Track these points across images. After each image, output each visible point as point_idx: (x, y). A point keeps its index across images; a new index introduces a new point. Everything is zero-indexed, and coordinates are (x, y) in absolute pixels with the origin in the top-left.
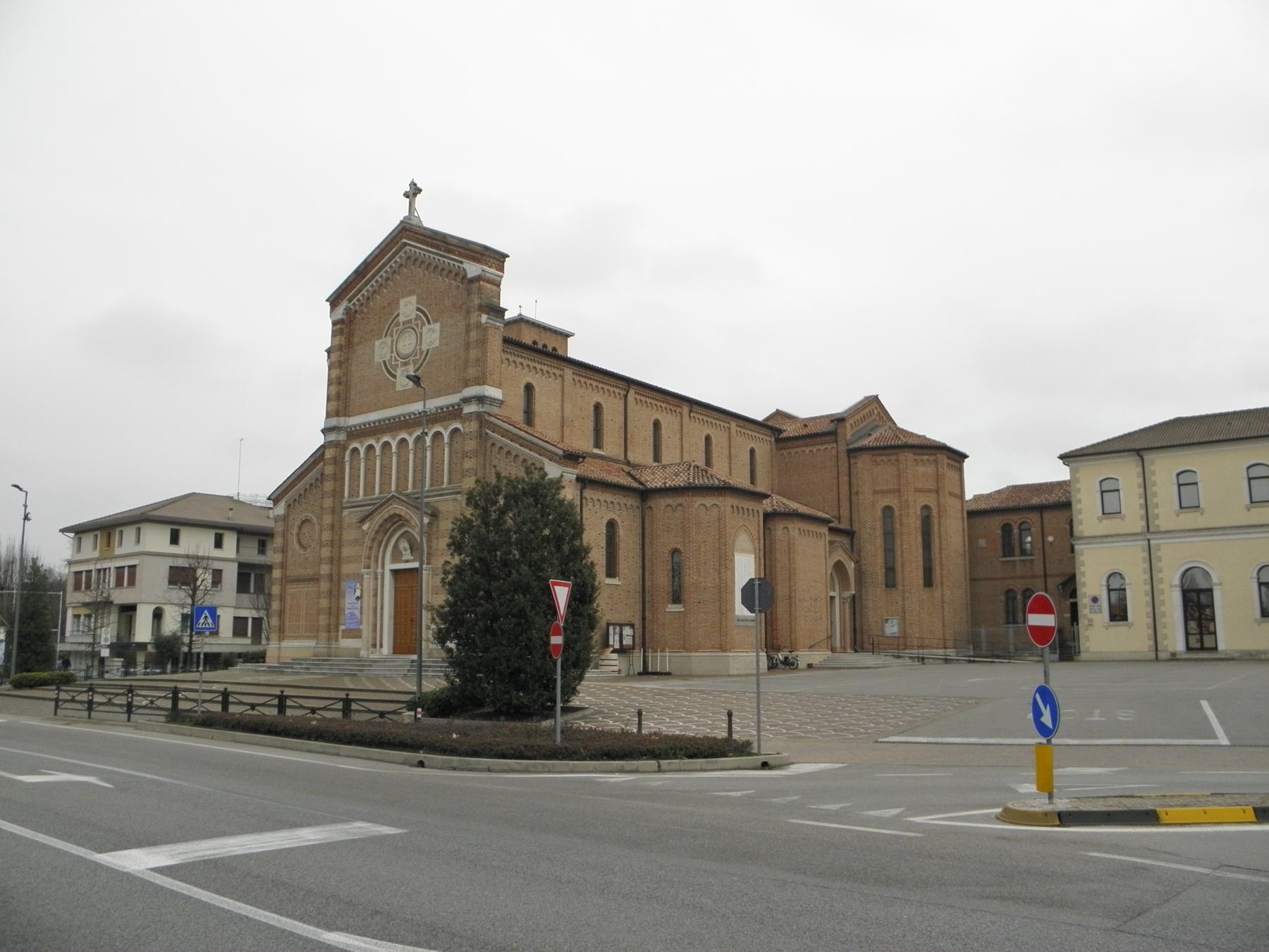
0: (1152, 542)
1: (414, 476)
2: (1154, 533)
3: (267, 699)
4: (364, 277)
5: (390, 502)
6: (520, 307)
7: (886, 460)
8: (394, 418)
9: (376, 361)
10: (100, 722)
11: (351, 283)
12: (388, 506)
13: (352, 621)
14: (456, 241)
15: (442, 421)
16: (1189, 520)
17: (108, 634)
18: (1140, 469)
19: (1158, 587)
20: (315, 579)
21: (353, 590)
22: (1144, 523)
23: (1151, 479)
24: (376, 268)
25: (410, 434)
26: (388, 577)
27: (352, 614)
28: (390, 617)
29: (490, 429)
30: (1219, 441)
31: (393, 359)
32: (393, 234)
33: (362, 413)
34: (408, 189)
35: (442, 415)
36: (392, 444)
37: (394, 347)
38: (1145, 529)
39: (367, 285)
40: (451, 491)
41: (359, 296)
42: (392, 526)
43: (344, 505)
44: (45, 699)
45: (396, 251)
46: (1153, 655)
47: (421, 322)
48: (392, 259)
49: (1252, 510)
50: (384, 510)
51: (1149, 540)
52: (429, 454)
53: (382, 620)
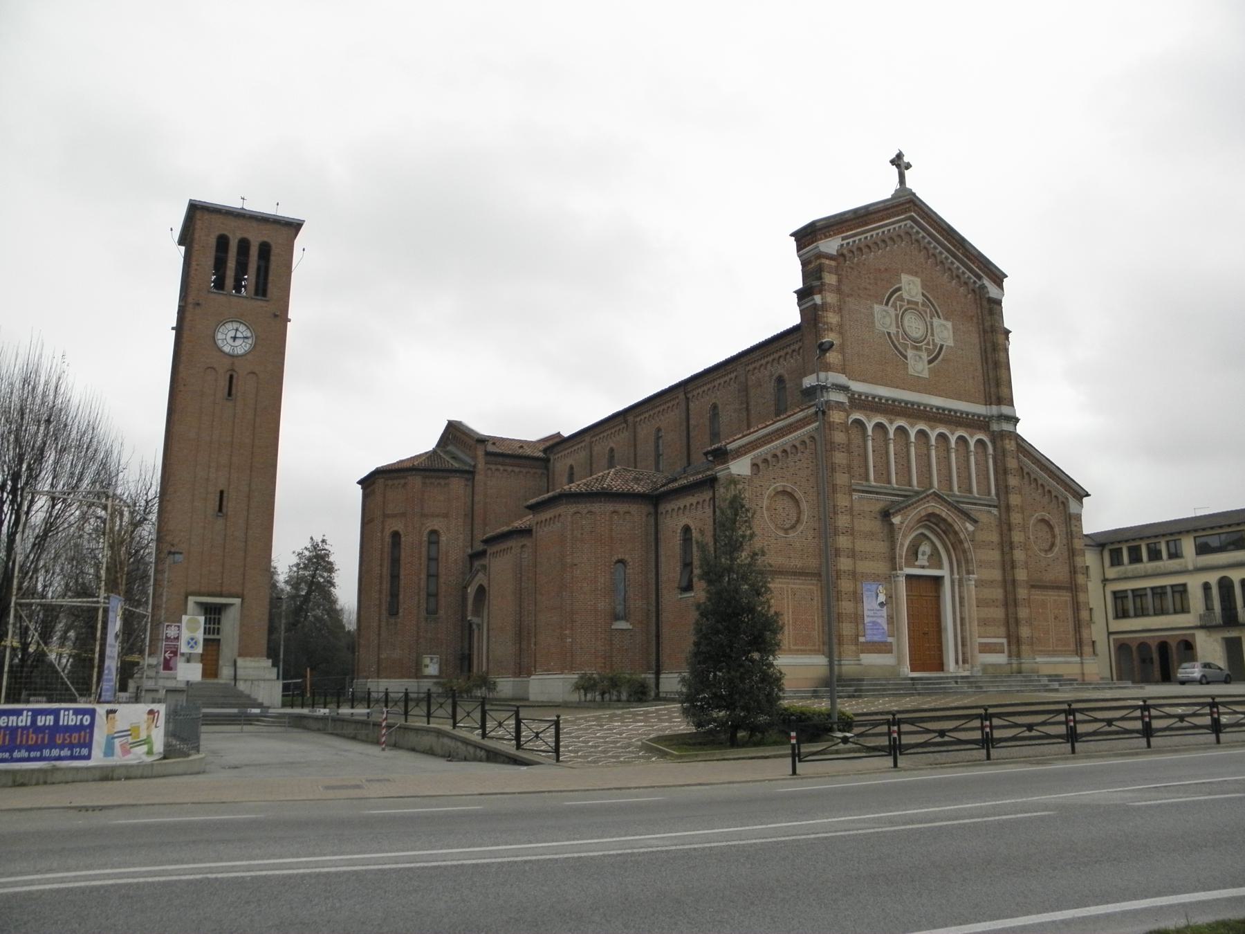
1: (996, 485)
3: (968, 725)
7: (436, 483)
8: (900, 401)
10: (1160, 751)
11: (847, 221)
12: (924, 503)
13: (875, 632)
15: (909, 417)
17: (197, 629)
21: (874, 596)
24: (946, 242)
26: (902, 583)
27: (874, 623)
28: (946, 629)
35: (857, 401)
36: (931, 435)
37: (929, 327)
40: (986, 503)
43: (854, 487)
53: (956, 636)
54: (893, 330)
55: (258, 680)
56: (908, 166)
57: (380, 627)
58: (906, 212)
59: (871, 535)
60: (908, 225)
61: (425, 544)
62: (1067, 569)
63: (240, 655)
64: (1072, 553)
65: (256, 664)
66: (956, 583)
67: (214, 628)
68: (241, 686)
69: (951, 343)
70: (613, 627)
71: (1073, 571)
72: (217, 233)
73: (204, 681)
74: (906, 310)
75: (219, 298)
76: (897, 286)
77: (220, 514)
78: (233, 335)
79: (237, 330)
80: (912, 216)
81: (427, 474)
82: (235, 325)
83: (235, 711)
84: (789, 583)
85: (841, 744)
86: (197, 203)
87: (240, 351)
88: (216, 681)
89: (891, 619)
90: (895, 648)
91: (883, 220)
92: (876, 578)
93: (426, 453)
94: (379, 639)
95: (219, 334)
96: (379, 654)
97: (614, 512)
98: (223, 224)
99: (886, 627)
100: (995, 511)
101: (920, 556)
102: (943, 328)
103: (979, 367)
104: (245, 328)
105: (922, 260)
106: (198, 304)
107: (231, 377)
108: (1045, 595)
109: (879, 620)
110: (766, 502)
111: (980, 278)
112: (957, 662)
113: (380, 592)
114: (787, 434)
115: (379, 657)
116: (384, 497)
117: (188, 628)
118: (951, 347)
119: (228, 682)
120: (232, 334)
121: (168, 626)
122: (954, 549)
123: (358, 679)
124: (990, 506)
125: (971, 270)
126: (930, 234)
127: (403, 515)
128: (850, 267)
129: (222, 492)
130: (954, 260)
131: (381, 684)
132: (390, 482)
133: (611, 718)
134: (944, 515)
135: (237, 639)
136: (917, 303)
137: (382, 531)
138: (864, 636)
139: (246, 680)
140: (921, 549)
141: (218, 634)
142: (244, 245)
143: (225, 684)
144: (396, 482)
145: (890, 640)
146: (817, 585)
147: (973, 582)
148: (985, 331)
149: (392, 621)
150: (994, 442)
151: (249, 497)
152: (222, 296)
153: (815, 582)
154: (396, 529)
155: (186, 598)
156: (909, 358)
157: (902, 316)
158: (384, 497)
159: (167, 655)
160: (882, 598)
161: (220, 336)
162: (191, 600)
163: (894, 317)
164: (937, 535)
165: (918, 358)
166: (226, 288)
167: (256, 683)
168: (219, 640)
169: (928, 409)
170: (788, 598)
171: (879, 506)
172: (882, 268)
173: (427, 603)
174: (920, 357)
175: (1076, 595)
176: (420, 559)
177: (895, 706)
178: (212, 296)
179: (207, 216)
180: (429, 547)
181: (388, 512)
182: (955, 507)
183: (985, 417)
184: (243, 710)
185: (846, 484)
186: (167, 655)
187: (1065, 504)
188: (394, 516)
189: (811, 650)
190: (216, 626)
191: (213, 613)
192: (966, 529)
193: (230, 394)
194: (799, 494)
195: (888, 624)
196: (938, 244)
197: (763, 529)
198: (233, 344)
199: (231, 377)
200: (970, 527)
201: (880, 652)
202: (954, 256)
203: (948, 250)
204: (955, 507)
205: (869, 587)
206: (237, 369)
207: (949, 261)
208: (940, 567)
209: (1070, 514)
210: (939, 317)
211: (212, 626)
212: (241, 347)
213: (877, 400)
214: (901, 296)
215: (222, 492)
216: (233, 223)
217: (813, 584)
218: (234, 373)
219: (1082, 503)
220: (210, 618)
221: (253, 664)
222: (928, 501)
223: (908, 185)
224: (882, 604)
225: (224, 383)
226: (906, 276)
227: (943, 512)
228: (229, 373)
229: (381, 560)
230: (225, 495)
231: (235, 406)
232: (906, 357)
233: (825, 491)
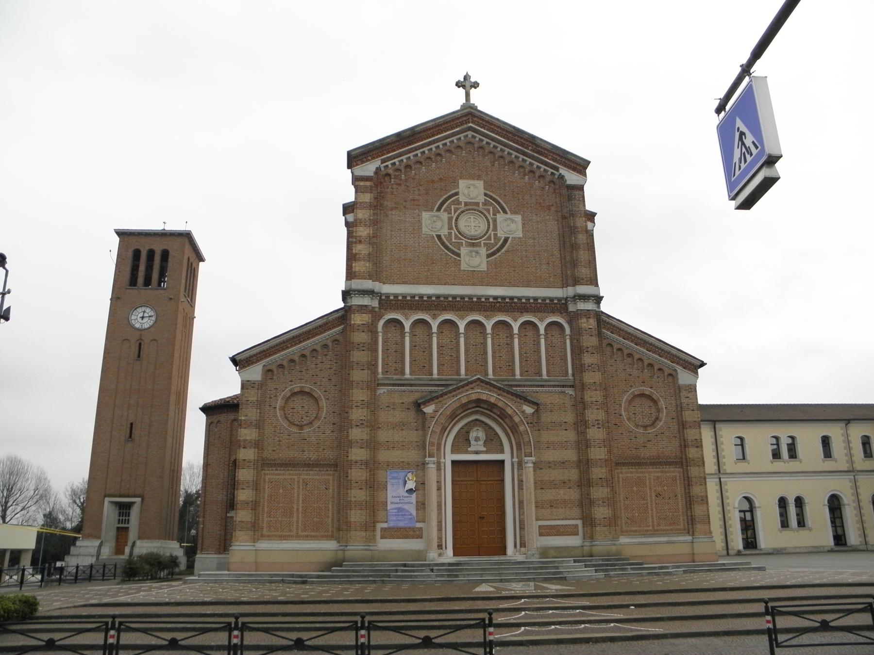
0: (722, 480)
2: (723, 474)
4: (410, 145)
5: (471, 386)
6: (165, 223)
9: (423, 232)
11: (388, 144)
14: (551, 147)
16: (742, 467)
18: (712, 433)
19: (727, 508)
20: (264, 464)
21: (401, 482)
22: (716, 467)
23: (720, 440)
25: (435, 317)
29: (608, 330)
30: (785, 420)
31: (453, 236)
32: (456, 114)
33: (404, 283)
34: (473, 80)
38: (717, 472)
39: (410, 152)
40: (557, 383)
41: (396, 160)
42: (462, 413)
43: (381, 382)
44: (748, 633)
45: (457, 131)
46: (725, 552)
47: (493, 209)
48: (449, 138)
49: (774, 463)
50: (460, 393)
51: (720, 478)
52: (462, 340)
54: (444, 232)
56: (475, 85)
58: (462, 124)
59: (402, 426)
60: (470, 136)
62: (676, 443)
63: (140, 538)
64: (683, 425)
66: (516, 466)
67: (125, 520)
69: (519, 234)
70: (228, 515)
71: (684, 445)
72: (133, 249)
74: (462, 212)
75: (133, 292)
76: (456, 191)
77: (130, 439)
78: (142, 316)
79: (144, 312)
80: (471, 127)
82: (143, 309)
84: (300, 474)
85: (179, 638)
87: (146, 326)
89: (421, 505)
90: (425, 533)
91: (433, 135)
92: (405, 466)
97: (234, 420)
98: (136, 241)
99: (414, 513)
100: (570, 391)
101: (473, 442)
102: (509, 222)
103: (556, 253)
104: (150, 310)
105: (489, 164)
107: (140, 344)
108: (642, 472)
109: (406, 507)
110: (280, 403)
111: (557, 169)
112: (515, 546)
114: (304, 341)
118: (520, 238)
120: (141, 315)
122: (513, 434)
124: (563, 386)
125: (546, 164)
126: (493, 139)
128: (397, 184)
129: (132, 424)
130: (525, 158)
133: (257, 598)
134: (492, 400)
136: (477, 204)
138: (386, 522)
140: (473, 435)
141: (128, 523)
142: (151, 254)
145: (419, 525)
146: (334, 475)
147: (532, 465)
148: (564, 217)
150: (570, 323)
152: (135, 291)
153: (331, 472)
156: (462, 255)
157: (456, 220)
160: (411, 485)
163: (446, 220)
164: (494, 420)
165: (474, 254)
166: (138, 285)
169: (483, 300)
170: (299, 488)
171: (412, 398)
172: (436, 178)
174: (477, 252)
175: (687, 470)
177: (208, 597)
178: (128, 291)
182: (507, 391)
183: (559, 299)
185: (365, 379)
187: (673, 376)
189: (323, 536)
190: (127, 518)
191: (124, 509)
192: (523, 412)
193: (139, 356)
194: (318, 393)
195: (417, 509)
196: (504, 146)
197: (275, 427)
199: (140, 344)
200: (529, 410)
201: (406, 537)
202: (525, 154)
203: (517, 150)
204: (507, 391)
205: (395, 475)
206: (143, 338)
207: (520, 159)
208: (502, 451)
209: (679, 385)
210: (505, 212)
211: (124, 518)
212: (147, 323)
213: (417, 298)
214: (458, 200)
215: (132, 424)
216: (143, 240)
217: (329, 475)
218: (143, 343)
219: (697, 373)
222: (472, 388)
223: (472, 101)
224: (410, 491)
225: (134, 349)
226: (464, 181)
227: (493, 397)
228: (139, 342)
230: (134, 426)
232: (459, 255)
233: (344, 386)
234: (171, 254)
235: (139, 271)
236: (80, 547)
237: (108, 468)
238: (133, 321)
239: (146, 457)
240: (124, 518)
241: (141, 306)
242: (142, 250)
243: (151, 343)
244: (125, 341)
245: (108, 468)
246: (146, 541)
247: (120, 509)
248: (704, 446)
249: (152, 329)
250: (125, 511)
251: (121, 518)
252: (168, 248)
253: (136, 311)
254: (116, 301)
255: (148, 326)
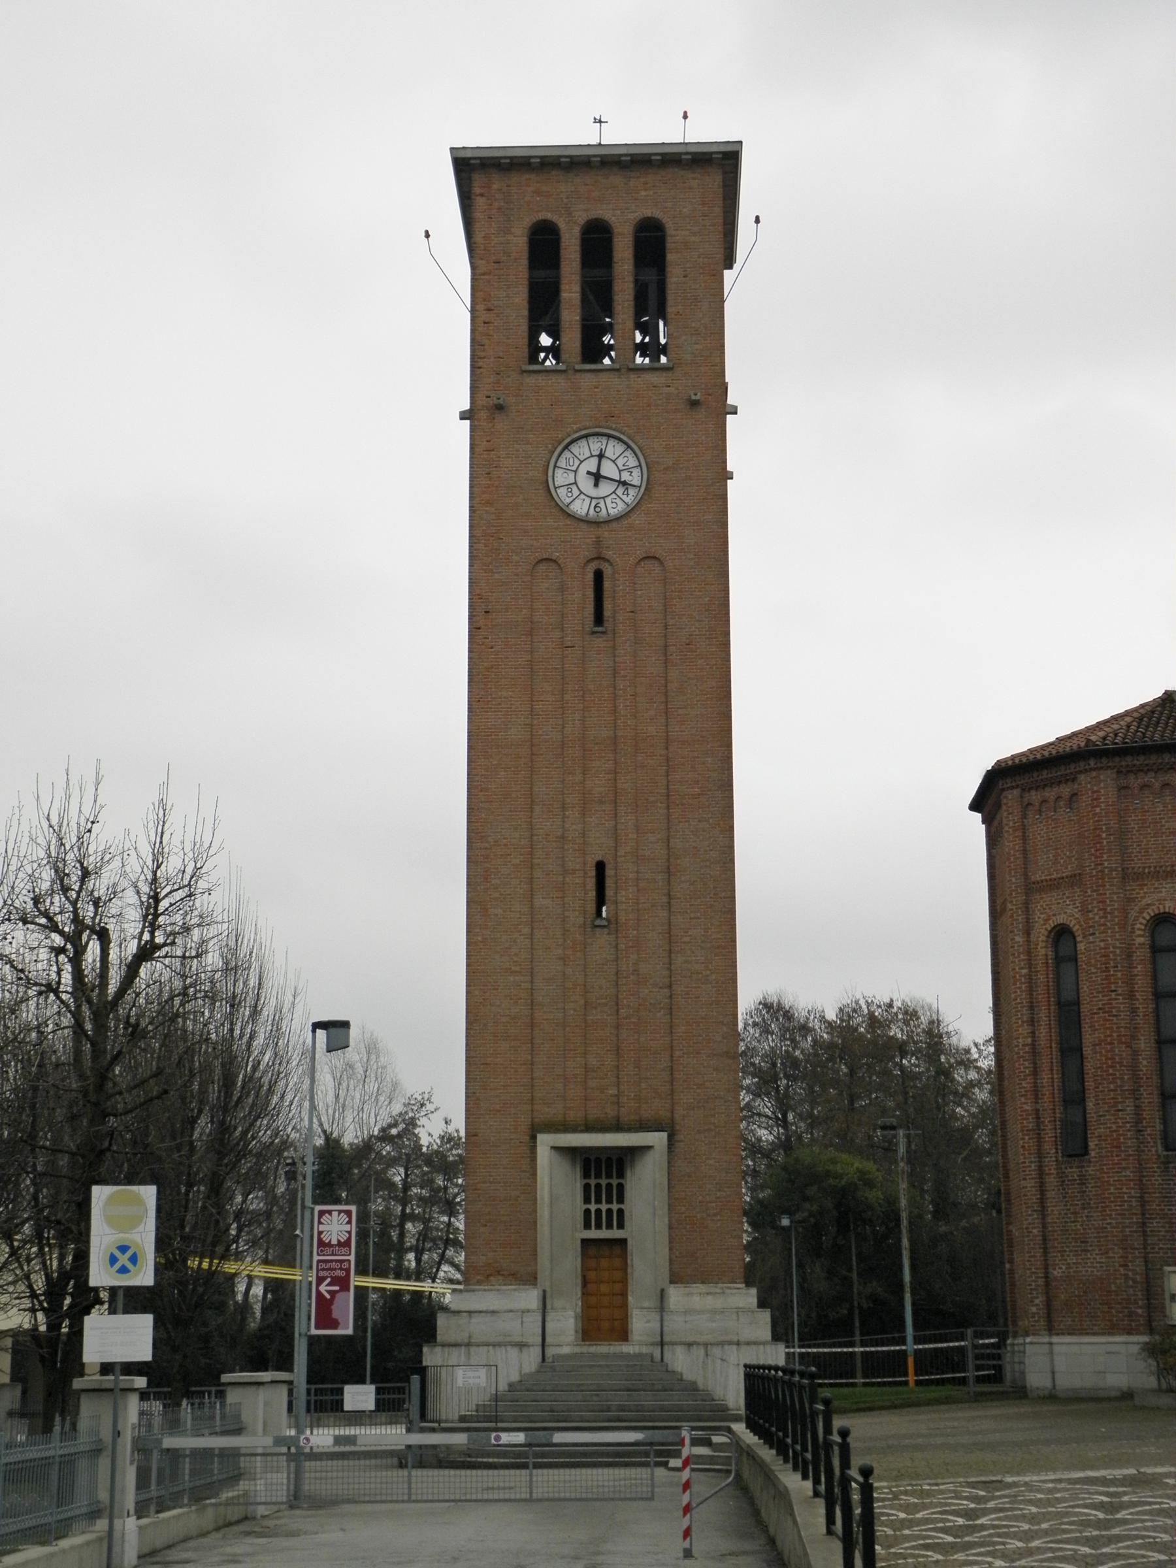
7: (1157, 785)
55: (722, 1344)
57: (1042, 1189)
61: (1142, 954)
65: (717, 1302)
68: (680, 1361)
72: (528, 220)
73: (585, 1349)
79: (601, 456)
81: (1129, 760)
82: (596, 445)
83: (558, 1437)
86: (469, 154)
87: (614, 507)
88: (627, 1349)
93: (1127, 713)
94: (1044, 1226)
95: (559, 472)
96: (1046, 1267)
98: (538, 192)
104: (620, 448)
106: (500, 408)
107: (599, 576)
113: (1036, 1093)
115: (1046, 1276)
116: (1024, 838)
117: (109, 1220)
119: (644, 1350)
120: (592, 465)
121: (321, 1213)
123: (1015, 1336)
127: (1075, 880)
129: (600, 867)
131: (1056, 1349)
132: (1035, 797)
135: (664, 1239)
137: (1028, 933)
139: (690, 1345)
141: (621, 1226)
143: (639, 1356)
144: (1050, 794)
149: (1073, 1172)
151: (668, 871)
154: (1061, 919)
155: (534, 1138)
158: (1024, 838)
159: (323, 1288)
161: (561, 478)
162: (545, 1141)
167: (716, 1351)
168: (623, 1242)
173: (1164, 1121)
176: (1131, 995)
179: (498, 182)
180: (1154, 962)
181: (1038, 876)
184: (540, 1436)
186: (323, 1288)
188: (1052, 885)
190: (615, 1207)
193: (599, 619)
198: (593, 492)
199: (599, 576)
206: (609, 554)
215: (600, 867)
216: (563, 186)
218: (607, 570)
220: (598, 1186)
221: (710, 1302)
225: (581, 596)
228: (592, 567)
229: (1031, 1008)
230: (609, 872)
231: (614, 648)
234: (675, 236)
235: (563, 306)
236: (470, 1312)
237: (532, 1025)
238: (562, 492)
239: (670, 987)
240: (604, 1207)
241: (586, 436)
242: (562, 225)
243: (639, 570)
244: (542, 567)
245: (532, 1025)
246: (702, 1288)
247: (586, 1175)
248: (435, 1443)
249: (637, 519)
250: (604, 1182)
251: (593, 1207)
252: (656, 213)
253: (567, 454)
254: (491, 419)
255: (621, 507)
